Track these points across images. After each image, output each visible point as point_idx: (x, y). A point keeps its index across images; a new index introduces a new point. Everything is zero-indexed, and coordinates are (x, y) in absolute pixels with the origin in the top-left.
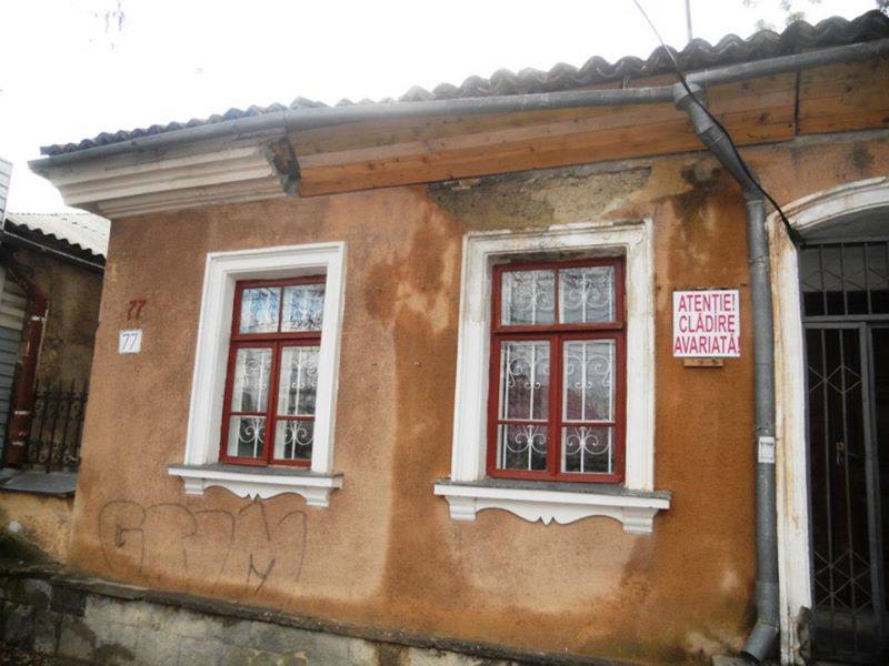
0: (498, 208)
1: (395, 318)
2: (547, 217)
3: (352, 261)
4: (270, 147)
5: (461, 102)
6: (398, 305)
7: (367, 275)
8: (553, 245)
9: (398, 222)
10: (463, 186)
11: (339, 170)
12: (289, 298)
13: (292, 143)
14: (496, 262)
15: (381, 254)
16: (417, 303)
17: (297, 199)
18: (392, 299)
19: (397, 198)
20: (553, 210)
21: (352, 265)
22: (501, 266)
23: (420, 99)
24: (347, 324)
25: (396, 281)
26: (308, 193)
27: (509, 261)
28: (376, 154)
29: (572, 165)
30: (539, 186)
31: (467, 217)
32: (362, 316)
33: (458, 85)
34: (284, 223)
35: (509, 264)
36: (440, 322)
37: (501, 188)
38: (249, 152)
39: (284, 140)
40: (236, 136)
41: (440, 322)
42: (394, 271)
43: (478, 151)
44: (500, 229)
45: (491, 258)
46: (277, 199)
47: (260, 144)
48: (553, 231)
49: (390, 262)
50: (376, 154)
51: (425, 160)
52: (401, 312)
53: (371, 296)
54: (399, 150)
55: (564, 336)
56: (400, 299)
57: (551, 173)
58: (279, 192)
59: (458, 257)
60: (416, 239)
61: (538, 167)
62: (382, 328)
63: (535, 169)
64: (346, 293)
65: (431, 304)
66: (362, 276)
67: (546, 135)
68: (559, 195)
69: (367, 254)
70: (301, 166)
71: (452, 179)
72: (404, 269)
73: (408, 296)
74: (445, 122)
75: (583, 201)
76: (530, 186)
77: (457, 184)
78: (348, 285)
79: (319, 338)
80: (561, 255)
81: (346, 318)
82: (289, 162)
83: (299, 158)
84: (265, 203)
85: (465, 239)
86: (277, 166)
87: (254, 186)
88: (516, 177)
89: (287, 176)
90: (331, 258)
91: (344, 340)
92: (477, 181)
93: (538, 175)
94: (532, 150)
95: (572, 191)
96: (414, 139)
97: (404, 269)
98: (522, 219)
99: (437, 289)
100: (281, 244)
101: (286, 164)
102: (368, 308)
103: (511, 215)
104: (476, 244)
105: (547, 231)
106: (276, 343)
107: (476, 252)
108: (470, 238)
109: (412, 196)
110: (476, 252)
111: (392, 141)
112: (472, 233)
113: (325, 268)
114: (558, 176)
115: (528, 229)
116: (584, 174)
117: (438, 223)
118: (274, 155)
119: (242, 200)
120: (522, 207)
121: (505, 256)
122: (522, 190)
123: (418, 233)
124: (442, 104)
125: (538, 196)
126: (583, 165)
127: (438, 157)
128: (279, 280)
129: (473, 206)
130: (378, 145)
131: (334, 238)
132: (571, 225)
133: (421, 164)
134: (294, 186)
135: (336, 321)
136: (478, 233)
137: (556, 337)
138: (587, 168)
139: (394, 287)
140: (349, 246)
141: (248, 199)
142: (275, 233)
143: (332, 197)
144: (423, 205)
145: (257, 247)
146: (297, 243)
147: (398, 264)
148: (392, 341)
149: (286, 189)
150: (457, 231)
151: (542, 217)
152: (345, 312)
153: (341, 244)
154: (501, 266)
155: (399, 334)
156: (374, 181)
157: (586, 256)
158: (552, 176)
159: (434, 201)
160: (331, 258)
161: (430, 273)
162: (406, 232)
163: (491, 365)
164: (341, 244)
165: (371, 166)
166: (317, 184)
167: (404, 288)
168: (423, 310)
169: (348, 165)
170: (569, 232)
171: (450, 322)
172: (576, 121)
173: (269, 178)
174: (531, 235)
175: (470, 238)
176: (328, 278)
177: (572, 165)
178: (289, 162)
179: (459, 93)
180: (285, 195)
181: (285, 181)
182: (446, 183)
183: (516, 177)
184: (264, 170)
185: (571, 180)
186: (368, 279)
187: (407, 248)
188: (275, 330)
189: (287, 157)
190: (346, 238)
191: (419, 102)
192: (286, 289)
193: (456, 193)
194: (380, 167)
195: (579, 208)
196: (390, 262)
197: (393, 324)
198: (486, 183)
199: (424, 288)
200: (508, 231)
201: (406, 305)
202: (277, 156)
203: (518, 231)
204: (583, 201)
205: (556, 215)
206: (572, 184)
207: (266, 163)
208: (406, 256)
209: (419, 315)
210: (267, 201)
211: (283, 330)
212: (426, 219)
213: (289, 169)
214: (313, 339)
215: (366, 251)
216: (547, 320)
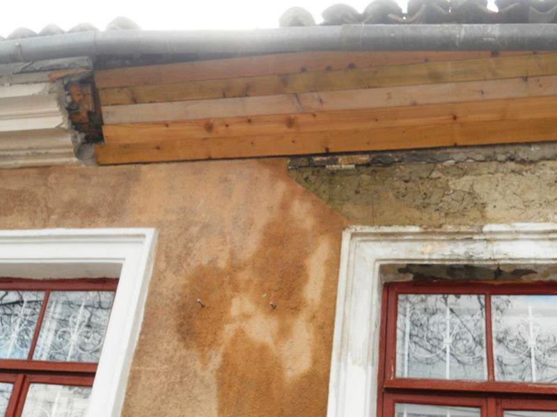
0: (397, 198)
1: (222, 349)
2: (475, 213)
3: (163, 257)
4: (66, 87)
5: (363, 30)
6: (229, 331)
7: (183, 281)
8: (487, 256)
9: (238, 210)
10: (343, 164)
11: (164, 129)
12: (55, 311)
13: (98, 85)
14: (391, 278)
15: (209, 252)
16: (261, 329)
17: (92, 167)
18: (221, 319)
19: (239, 174)
20: (484, 205)
21: (162, 265)
22: (397, 284)
23: (300, 24)
24: (142, 352)
25: (229, 293)
26: (111, 160)
27: (410, 277)
28: (218, 109)
29: (512, 144)
30: (461, 170)
31: (349, 208)
32: (169, 343)
33: (360, 10)
34: (66, 198)
35: (407, 283)
36: (296, 360)
37: (403, 170)
38: (36, 89)
39: (87, 81)
40: (20, 66)
41: (296, 360)
42: (227, 279)
43: (373, 115)
44: (404, 225)
45: (384, 270)
46: (61, 167)
47: (53, 81)
48: (491, 232)
49: (222, 264)
50: (218, 109)
51: (290, 122)
52: (234, 342)
53: (187, 313)
54: (255, 105)
55: (506, 403)
56: (233, 320)
57: (480, 154)
58: (69, 155)
59: (334, 264)
60: (265, 234)
61: (460, 143)
62: (198, 365)
63: (456, 146)
64: (148, 305)
65: (284, 333)
66: (175, 283)
67: (478, 96)
68: (494, 185)
69: (188, 251)
70: (106, 120)
71: (327, 154)
72: (243, 276)
73: (246, 317)
74: (329, 69)
75: (533, 196)
76: (445, 171)
77: (335, 162)
78: (152, 293)
79: (93, 375)
80: (498, 272)
81: (141, 343)
82: (89, 113)
83: (105, 109)
84: (45, 169)
85: (346, 236)
86: (70, 118)
87: (34, 143)
88: (426, 155)
89: (83, 135)
90: (131, 252)
91: (134, 379)
92: (365, 158)
93: (459, 155)
94: (455, 118)
95: (515, 179)
96: (277, 91)
97: (243, 276)
98: (436, 215)
99: (296, 310)
100: (58, 225)
101: (84, 114)
102: (178, 331)
103: (418, 208)
104: (363, 245)
105: (481, 233)
106: (21, 377)
107: (363, 259)
108: (354, 235)
109: (266, 173)
110: (363, 259)
111: (246, 92)
112: (359, 229)
113: (118, 267)
114: (489, 159)
115: (450, 228)
116: (531, 158)
117: (303, 213)
118: (69, 99)
119: (11, 163)
120: (434, 199)
121: (407, 269)
122: (434, 175)
123: (269, 226)
124: (336, 31)
125: (463, 183)
126: (529, 144)
127: (311, 119)
128: (44, 281)
129: (357, 192)
130: (224, 96)
131: (137, 224)
132: (520, 226)
133: (284, 128)
134: (91, 150)
135: (125, 346)
136: (367, 229)
137: (492, 403)
138: (535, 151)
139: (225, 302)
140: (160, 236)
141: (21, 162)
142: (50, 212)
143: (144, 167)
144: (281, 187)
145: (22, 228)
146: (82, 227)
147: (235, 267)
148: (214, 387)
149: (79, 153)
150: (332, 226)
151: (473, 212)
152: (141, 334)
153: (150, 233)
154: (406, 282)
155: (227, 378)
156: (207, 150)
157: (536, 278)
158: (480, 157)
159: (299, 182)
160: (131, 252)
161: (283, 288)
162: (251, 223)
163: (544, 399)
164: (150, 233)
165: (209, 127)
166: (126, 146)
167: (241, 305)
168: (269, 340)
169: (175, 122)
170: (515, 236)
171: (315, 361)
172: (526, 79)
173: (57, 132)
174: (453, 237)
175: (354, 235)
176: (96, 375)
177: (512, 144)
178: (89, 113)
179: (359, 19)
180: (75, 160)
181: (79, 140)
182: (318, 159)
183: (426, 155)
184: (55, 119)
185: (512, 165)
186: (185, 287)
187: (251, 245)
188: (25, 357)
189: (88, 106)
190: (159, 225)
191: (299, 28)
192: (54, 296)
193: (333, 173)
194: (221, 129)
195: (527, 205)
196: (222, 264)
197: (216, 360)
198: (380, 161)
199: (274, 307)
200: (416, 229)
201: (243, 332)
202: (73, 102)
203: (431, 232)
204: (533, 196)
205: (490, 211)
206: (513, 171)
207: (54, 107)
208: (249, 256)
209: (263, 349)
210: (47, 167)
211: (36, 357)
212: (285, 207)
213: (88, 128)
214: (106, 282)
215: (185, 247)
216: (477, 374)
